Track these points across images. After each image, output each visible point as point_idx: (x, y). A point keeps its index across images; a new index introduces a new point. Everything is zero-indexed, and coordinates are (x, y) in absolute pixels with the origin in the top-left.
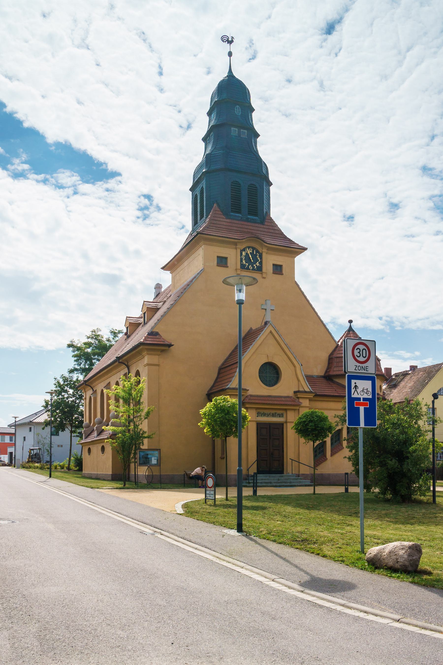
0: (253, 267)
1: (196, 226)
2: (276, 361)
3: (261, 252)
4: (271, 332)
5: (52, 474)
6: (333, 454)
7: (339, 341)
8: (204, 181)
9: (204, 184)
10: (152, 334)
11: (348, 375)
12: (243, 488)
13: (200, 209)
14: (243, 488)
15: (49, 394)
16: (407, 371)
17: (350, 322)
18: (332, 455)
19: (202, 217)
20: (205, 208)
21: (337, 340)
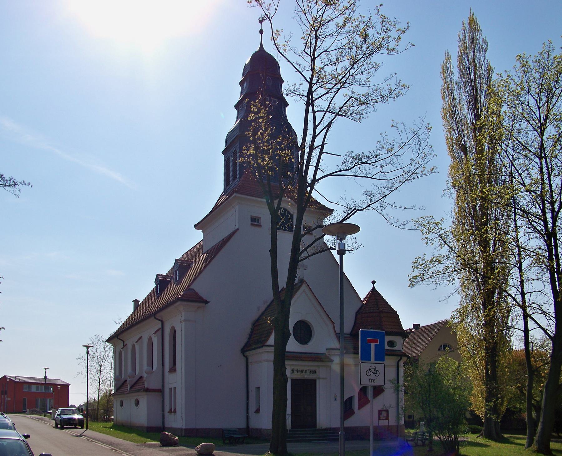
0: (285, 227)
1: (228, 188)
2: (308, 319)
3: (292, 213)
4: (304, 291)
5: (89, 426)
6: (361, 406)
7: (364, 301)
8: (238, 144)
9: (238, 146)
10: (189, 290)
11: (361, 331)
12: (287, 444)
13: (233, 171)
14: (287, 444)
15: (85, 348)
16: (410, 329)
17: (374, 282)
18: (359, 408)
19: (235, 178)
20: (238, 170)
21: (362, 299)
